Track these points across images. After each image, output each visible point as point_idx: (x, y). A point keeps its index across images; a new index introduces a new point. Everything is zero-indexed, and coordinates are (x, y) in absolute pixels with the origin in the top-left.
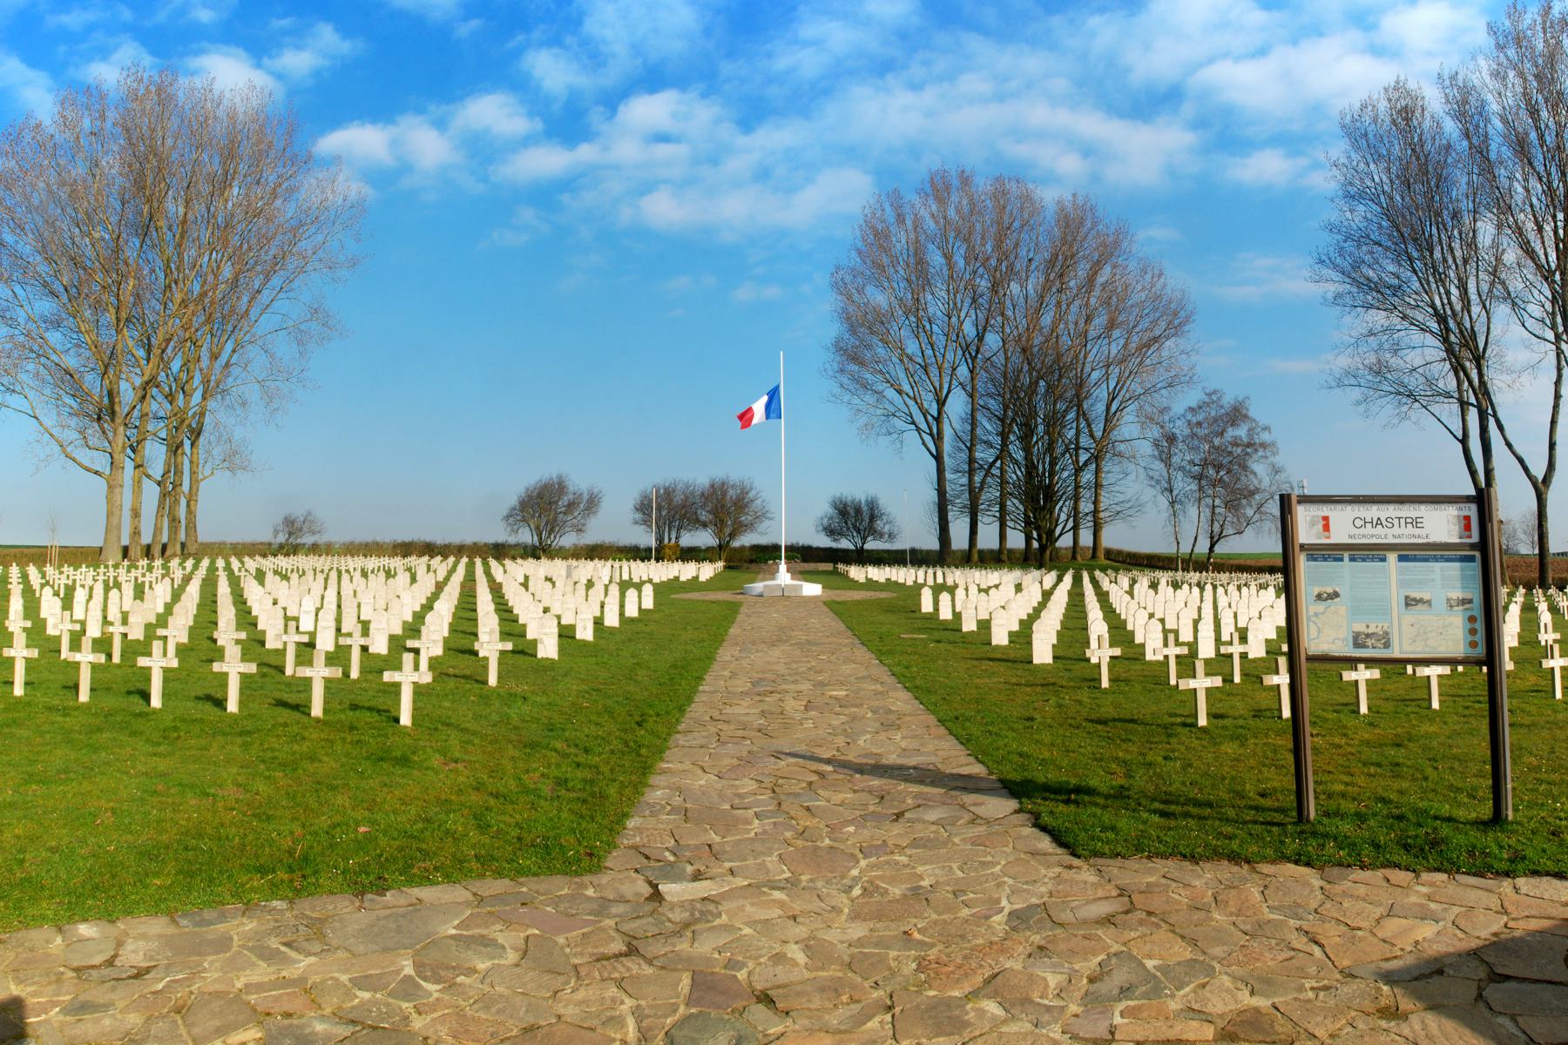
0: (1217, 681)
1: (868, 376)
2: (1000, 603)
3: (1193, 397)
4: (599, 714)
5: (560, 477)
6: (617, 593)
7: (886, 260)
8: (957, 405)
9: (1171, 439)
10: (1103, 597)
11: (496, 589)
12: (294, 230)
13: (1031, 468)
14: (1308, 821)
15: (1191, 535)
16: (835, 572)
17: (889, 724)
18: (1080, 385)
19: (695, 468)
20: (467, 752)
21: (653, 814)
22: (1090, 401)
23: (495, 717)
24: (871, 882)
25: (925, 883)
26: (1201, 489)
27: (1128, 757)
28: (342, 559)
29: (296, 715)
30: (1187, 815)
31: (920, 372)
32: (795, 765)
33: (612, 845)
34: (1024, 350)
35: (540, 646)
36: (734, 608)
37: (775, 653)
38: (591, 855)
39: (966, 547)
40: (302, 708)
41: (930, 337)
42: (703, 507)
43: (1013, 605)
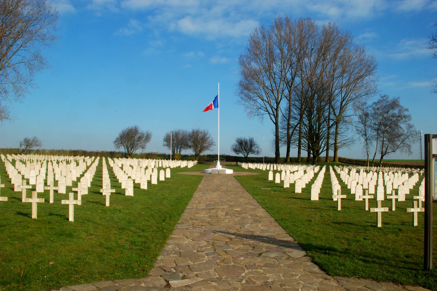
0: (387, 209)
1: (251, 94)
2: (296, 177)
3: (376, 98)
4: (149, 217)
5: (135, 127)
6: (157, 172)
7: (258, 52)
8: (284, 104)
9: (367, 115)
10: (338, 176)
11: (110, 170)
12: (27, 22)
13: (311, 128)
14: (429, 269)
15: (374, 151)
16: (237, 165)
17: (257, 220)
18: (331, 95)
19: (187, 126)
20: (96, 232)
21: (168, 254)
22: (335, 101)
23: (108, 218)
24: (249, 279)
25: (270, 280)
26: (378, 134)
27: (349, 237)
28: (49, 156)
29: (26, 218)
30: (374, 262)
31: (271, 92)
32: (222, 235)
33: (151, 267)
34: (309, 83)
35: (126, 191)
36: (199, 179)
37: (215, 194)
38: (144, 270)
39: (285, 156)
40: (28, 215)
41: (274, 80)
42: (190, 140)
43: (304, 178)
